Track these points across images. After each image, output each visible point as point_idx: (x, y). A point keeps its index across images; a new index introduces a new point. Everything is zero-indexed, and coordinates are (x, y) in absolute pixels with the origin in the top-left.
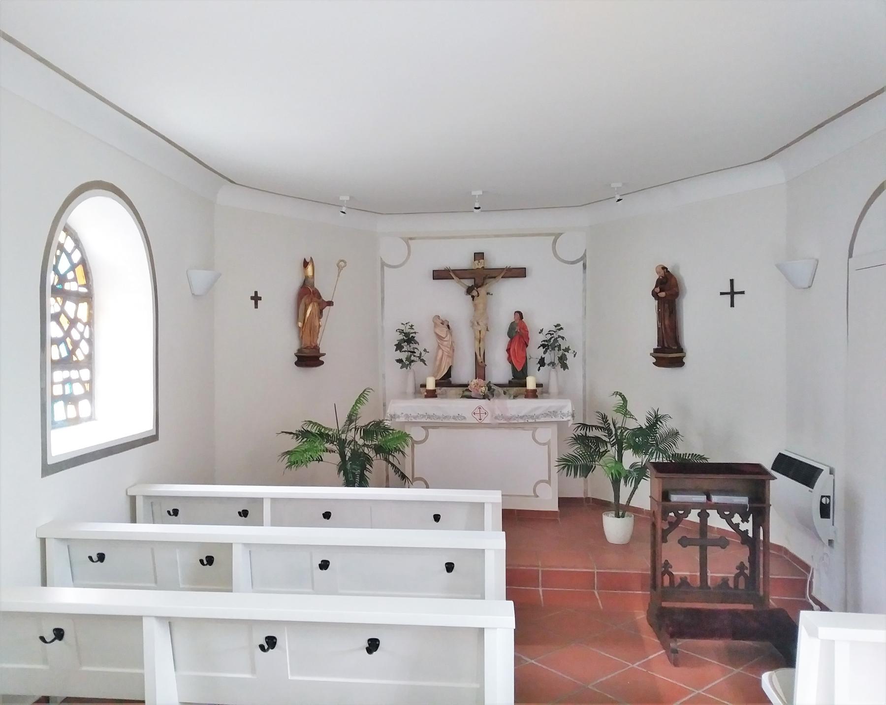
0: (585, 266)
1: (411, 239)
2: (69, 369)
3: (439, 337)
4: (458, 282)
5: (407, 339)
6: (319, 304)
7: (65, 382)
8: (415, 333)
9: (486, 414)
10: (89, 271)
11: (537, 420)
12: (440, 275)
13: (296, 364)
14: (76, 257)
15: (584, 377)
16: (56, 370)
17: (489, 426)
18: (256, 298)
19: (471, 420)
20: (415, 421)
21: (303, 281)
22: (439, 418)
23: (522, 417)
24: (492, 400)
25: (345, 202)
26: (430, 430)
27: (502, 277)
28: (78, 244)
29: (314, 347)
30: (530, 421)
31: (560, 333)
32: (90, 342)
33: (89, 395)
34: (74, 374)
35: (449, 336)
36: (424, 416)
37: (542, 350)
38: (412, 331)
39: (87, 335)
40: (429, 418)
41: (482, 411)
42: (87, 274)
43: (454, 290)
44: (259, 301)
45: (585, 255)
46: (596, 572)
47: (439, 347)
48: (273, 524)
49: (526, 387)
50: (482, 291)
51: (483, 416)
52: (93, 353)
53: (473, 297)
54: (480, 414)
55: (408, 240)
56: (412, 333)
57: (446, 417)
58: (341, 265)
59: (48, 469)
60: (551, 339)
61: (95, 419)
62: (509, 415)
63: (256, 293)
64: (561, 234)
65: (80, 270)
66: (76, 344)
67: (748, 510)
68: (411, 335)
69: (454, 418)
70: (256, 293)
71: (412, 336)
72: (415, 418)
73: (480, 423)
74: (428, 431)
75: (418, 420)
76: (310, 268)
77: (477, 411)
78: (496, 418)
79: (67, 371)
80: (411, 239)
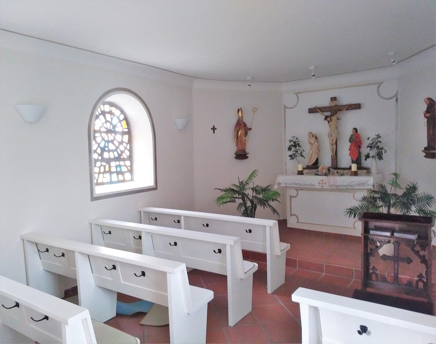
0: (397, 100)
1: (299, 93)
2: (119, 161)
3: (311, 143)
4: (321, 114)
5: (295, 144)
6: (245, 130)
7: (117, 166)
8: (298, 142)
9: (325, 183)
10: (129, 122)
11: (353, 188)
12: (312, 111)
13: (235, 158)
14: (122, 117)
15: (396, 164)
16: (112, 162)
17: (327, 190)
18: (214, 129)
19: (317, 186)
20: (290, 186)
21: (237, 120)
22: (301, 185)
23: (345, 186)
24: (329, 176)
25: (312, 70)
26: (299, 191)
27: (346, 110)
28: (122, 112)
29: (243, 150)
30: (350, 188)
31: (379, 139)
32: (131, 151)
33: (131, 171)
34: (122, 163)
35: (316, 142)
36: (294, 184)
37: (369, 148)
38: (297, 140)
39: (128, 147)
40: (297, 185)
41: (324, 182)
42: (128, 124)
43: (319, 117)
44: (215, 130)
45: (397, 93)
46: (354, 269)
47: (311, 149)
48: (185, 229)
49: (351, 169)
50: (334, 118)
51: (324, 185)
52: (132, 155)
53: (328, 122)
54: (322, 183)
55: (297, 94)
56: (298, 141)
57: (304, 185)
58: (255, 110)
59: (94, 198)
60: (373, 143)
61: (134, 181)
62: (337, 184)
63: (214, 126)
64: (382, 83)
65: (124, 123)
66: (122, 152)
67: (415, 243)
68: (297, 143)
69: (309, 185)
70: (214, 126)
71: (298, 143)
72: (289, 184)
73: (322, 188)
74: (298, 191)
75: (291, 186)
76: (240, 113)
77: (321, 182)
78: (331, 186)
79: (114, 162)
80: (299, 93)
